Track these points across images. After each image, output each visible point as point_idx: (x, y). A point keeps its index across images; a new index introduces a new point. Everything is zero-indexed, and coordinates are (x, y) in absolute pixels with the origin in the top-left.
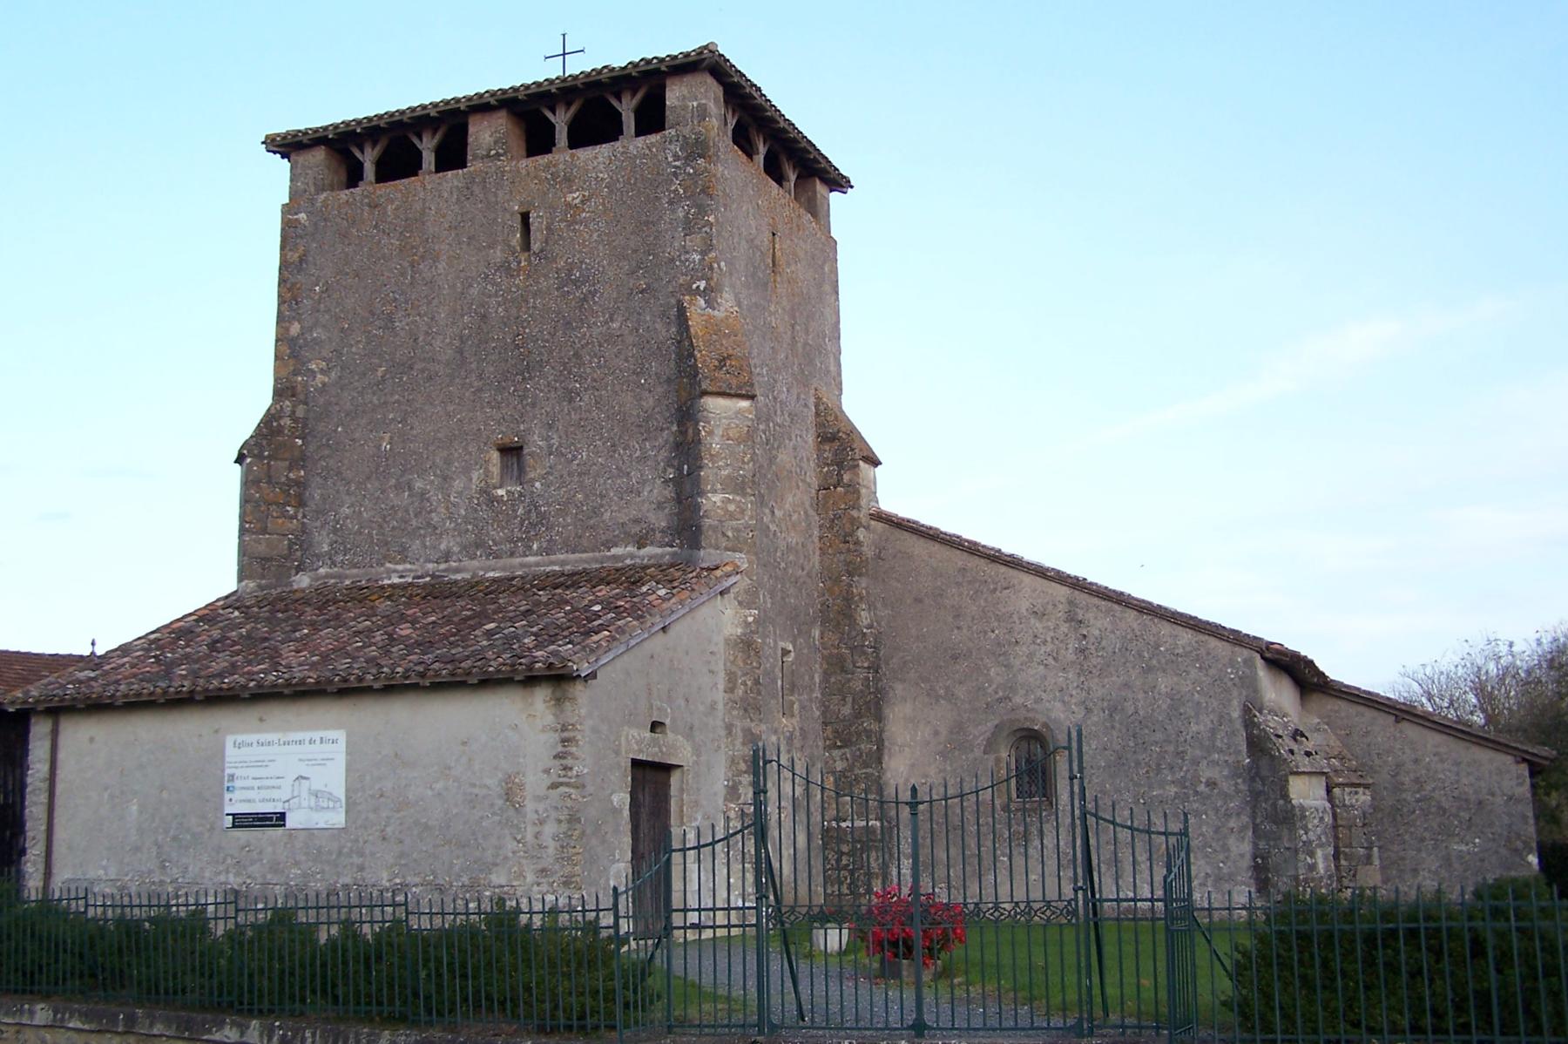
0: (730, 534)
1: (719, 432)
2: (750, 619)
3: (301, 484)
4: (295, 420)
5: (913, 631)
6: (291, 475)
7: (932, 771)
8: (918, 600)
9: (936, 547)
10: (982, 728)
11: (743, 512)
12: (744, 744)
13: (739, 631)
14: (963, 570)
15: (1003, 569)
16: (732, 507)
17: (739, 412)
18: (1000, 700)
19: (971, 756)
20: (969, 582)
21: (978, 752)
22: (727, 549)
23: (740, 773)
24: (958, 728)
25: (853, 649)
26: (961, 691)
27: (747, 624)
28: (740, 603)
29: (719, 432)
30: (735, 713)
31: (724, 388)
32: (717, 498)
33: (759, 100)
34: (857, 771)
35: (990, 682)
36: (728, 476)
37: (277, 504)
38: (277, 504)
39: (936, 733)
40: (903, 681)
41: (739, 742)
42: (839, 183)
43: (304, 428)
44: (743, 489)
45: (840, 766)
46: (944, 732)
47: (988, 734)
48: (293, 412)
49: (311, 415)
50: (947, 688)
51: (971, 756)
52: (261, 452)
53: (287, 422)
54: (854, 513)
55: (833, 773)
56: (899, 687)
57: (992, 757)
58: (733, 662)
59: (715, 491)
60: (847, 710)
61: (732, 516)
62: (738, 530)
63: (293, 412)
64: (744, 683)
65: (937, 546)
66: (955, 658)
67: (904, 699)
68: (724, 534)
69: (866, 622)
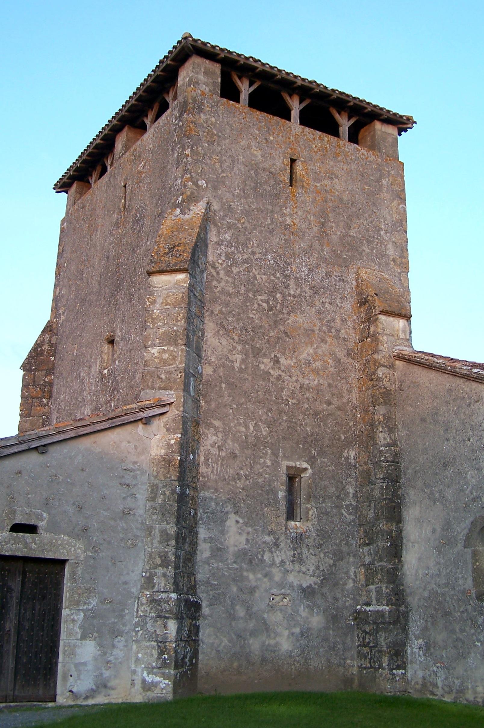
0: (163, 376)
1: (160, 300)
2: (173, 442)
3: (51, 384)
4: (51, 345)
5: (421, 446)
6: (46, 379)
7: (432, 564)
8: (423, 420)
9: (433, 375)
10: (463, 525)
11: (174, 358)
12: (160, 542)
13: (163, 452)
14: (450, 390)
15: (474, 385)
16: (166, 356)
17: (177, 283)
18: (474, 500)
19: (456, 550)
20: (454, 400)
21: (460, 546)
22: (160, 388)
23: (156, 566)
24: (448, 526)
25: (374, 464)
26: (449, 493)
27: (169, 446)
28: (168, 430)
29: (160, 300)
30: (155, 517)
31: (163, 266)
32: (155, 351)
33: (261, 68)
34: (377, 564)
35: (467, 483)
36: (164, 333)
37: (38, 398)
38: (38, 398)
39: (434, 531)
40: (414, 488)
41: (156, 541)
42: (401, 124)
43: (54, 350)
44: (176, 341)
45: (368, 560)
46: (439, 530)
47: (466, 530)
48: (50, 341)
49: (58, 342)
50: (440, 492)
51: (456, 550)
52: (31, 367)
53: (46, 347)
54: (376, 356)
55: (364, 565)
56: (412, 492)
57: (469, 551)
58: (156, 477)
59: (153, 346)
60: (371, 514)
61: (165, 362)
62: (170, 373)
63: (50, 341)
64: (164, 494)
65: (434, 373)
66: (445, 465)
67: (415, 503)
68: (159, 378)
69: (383, 442)
